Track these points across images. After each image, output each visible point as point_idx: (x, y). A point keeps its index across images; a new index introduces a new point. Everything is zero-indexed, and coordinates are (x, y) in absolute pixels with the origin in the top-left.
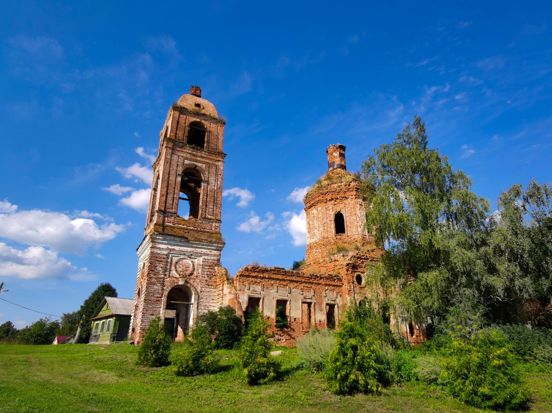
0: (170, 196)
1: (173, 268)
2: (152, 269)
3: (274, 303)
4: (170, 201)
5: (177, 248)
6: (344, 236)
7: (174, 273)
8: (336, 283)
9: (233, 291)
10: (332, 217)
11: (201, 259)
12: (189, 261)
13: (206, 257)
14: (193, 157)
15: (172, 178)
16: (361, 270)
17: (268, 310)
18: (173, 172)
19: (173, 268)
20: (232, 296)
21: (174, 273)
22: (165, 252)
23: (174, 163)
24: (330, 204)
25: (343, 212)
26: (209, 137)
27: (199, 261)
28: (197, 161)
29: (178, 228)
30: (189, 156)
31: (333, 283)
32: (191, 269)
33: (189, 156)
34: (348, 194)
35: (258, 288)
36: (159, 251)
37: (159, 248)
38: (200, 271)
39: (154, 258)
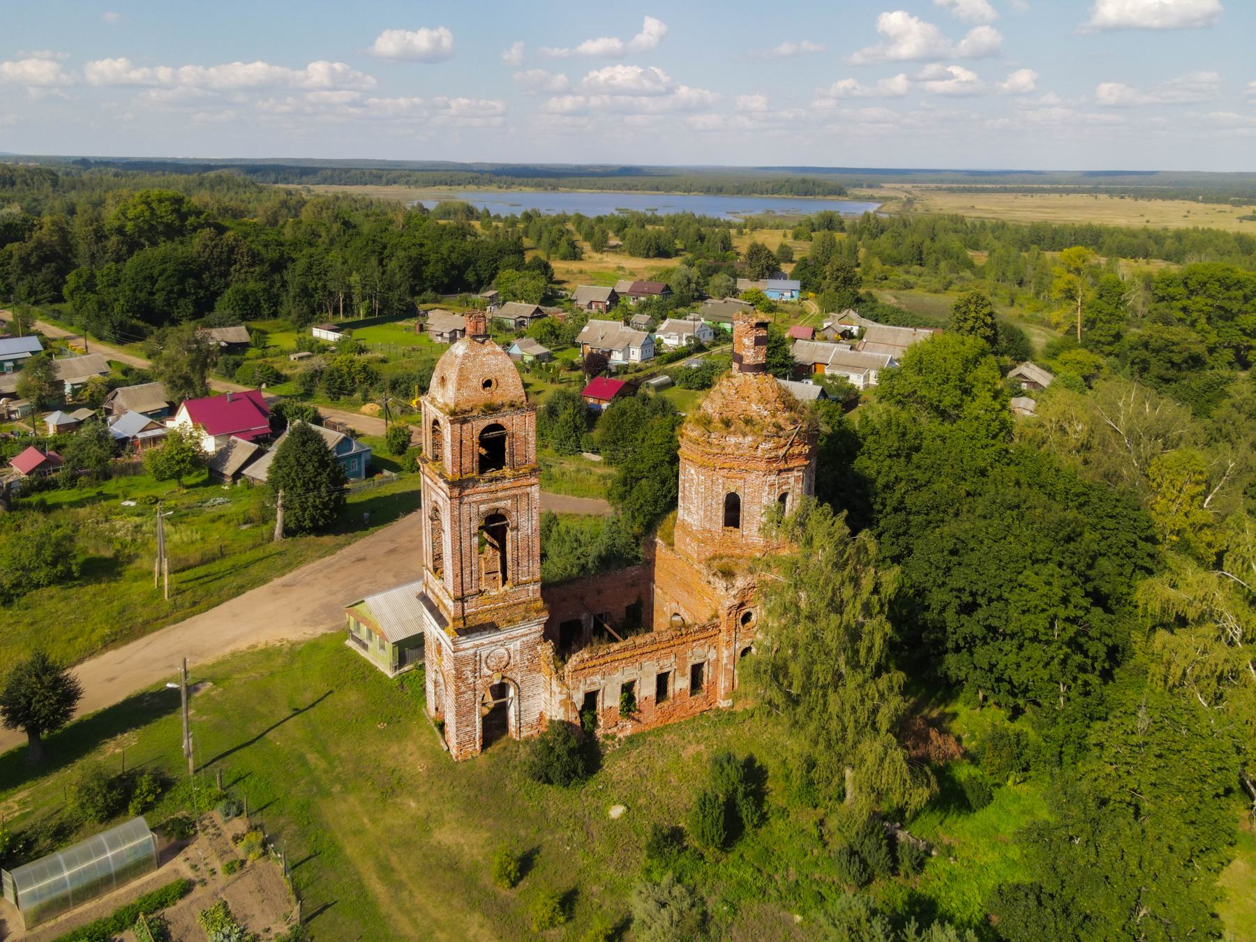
0: (467, 572)
1: (483, 665)
2: (459, 677)
3: (619, 689)
4: (467, 579)
5: (485, 641)
6: (735, 534)
7: (486, 671)
8: (711, 632)
9: (565, 690)
10: (722, 498)
11: (518, 643)
12: (502, 650)
13: (524, 639)
14: (491, 496)
15: (465, 544)
16: (752, 604)
17: (611, 700)
18: (465, 534)
19: (483, 665)
20: (564, 697)
21: (486, 671)
22: (472, 651)
23: (465, 518)
24: (719, 476)
25: (740, 494)
26: (512, 444)
27: (516, 646)
28: (498, 499)
29: (483, 612)
30: (485, 496)
31: (705, 635)
32: (506, 658)
33: (485, 496)
34: (751, 465)
35: (597, 678)
36: (463, 653)
37: (464, 650)
38: (518, 658)
39: (459, 663)
